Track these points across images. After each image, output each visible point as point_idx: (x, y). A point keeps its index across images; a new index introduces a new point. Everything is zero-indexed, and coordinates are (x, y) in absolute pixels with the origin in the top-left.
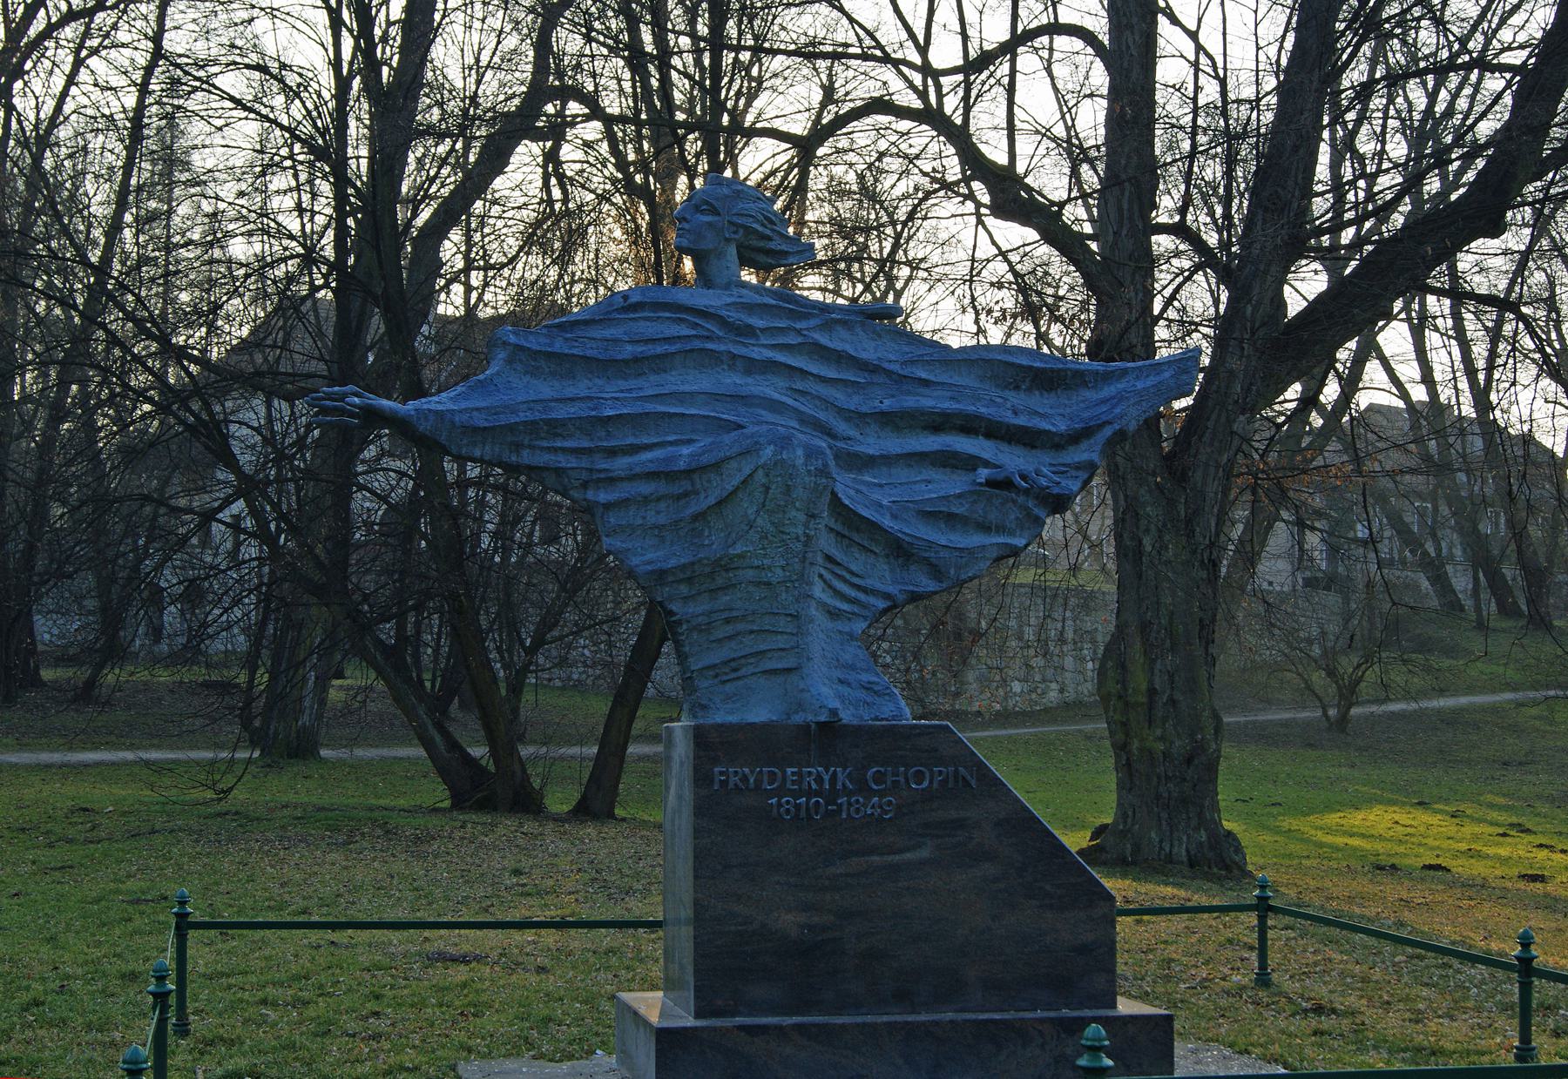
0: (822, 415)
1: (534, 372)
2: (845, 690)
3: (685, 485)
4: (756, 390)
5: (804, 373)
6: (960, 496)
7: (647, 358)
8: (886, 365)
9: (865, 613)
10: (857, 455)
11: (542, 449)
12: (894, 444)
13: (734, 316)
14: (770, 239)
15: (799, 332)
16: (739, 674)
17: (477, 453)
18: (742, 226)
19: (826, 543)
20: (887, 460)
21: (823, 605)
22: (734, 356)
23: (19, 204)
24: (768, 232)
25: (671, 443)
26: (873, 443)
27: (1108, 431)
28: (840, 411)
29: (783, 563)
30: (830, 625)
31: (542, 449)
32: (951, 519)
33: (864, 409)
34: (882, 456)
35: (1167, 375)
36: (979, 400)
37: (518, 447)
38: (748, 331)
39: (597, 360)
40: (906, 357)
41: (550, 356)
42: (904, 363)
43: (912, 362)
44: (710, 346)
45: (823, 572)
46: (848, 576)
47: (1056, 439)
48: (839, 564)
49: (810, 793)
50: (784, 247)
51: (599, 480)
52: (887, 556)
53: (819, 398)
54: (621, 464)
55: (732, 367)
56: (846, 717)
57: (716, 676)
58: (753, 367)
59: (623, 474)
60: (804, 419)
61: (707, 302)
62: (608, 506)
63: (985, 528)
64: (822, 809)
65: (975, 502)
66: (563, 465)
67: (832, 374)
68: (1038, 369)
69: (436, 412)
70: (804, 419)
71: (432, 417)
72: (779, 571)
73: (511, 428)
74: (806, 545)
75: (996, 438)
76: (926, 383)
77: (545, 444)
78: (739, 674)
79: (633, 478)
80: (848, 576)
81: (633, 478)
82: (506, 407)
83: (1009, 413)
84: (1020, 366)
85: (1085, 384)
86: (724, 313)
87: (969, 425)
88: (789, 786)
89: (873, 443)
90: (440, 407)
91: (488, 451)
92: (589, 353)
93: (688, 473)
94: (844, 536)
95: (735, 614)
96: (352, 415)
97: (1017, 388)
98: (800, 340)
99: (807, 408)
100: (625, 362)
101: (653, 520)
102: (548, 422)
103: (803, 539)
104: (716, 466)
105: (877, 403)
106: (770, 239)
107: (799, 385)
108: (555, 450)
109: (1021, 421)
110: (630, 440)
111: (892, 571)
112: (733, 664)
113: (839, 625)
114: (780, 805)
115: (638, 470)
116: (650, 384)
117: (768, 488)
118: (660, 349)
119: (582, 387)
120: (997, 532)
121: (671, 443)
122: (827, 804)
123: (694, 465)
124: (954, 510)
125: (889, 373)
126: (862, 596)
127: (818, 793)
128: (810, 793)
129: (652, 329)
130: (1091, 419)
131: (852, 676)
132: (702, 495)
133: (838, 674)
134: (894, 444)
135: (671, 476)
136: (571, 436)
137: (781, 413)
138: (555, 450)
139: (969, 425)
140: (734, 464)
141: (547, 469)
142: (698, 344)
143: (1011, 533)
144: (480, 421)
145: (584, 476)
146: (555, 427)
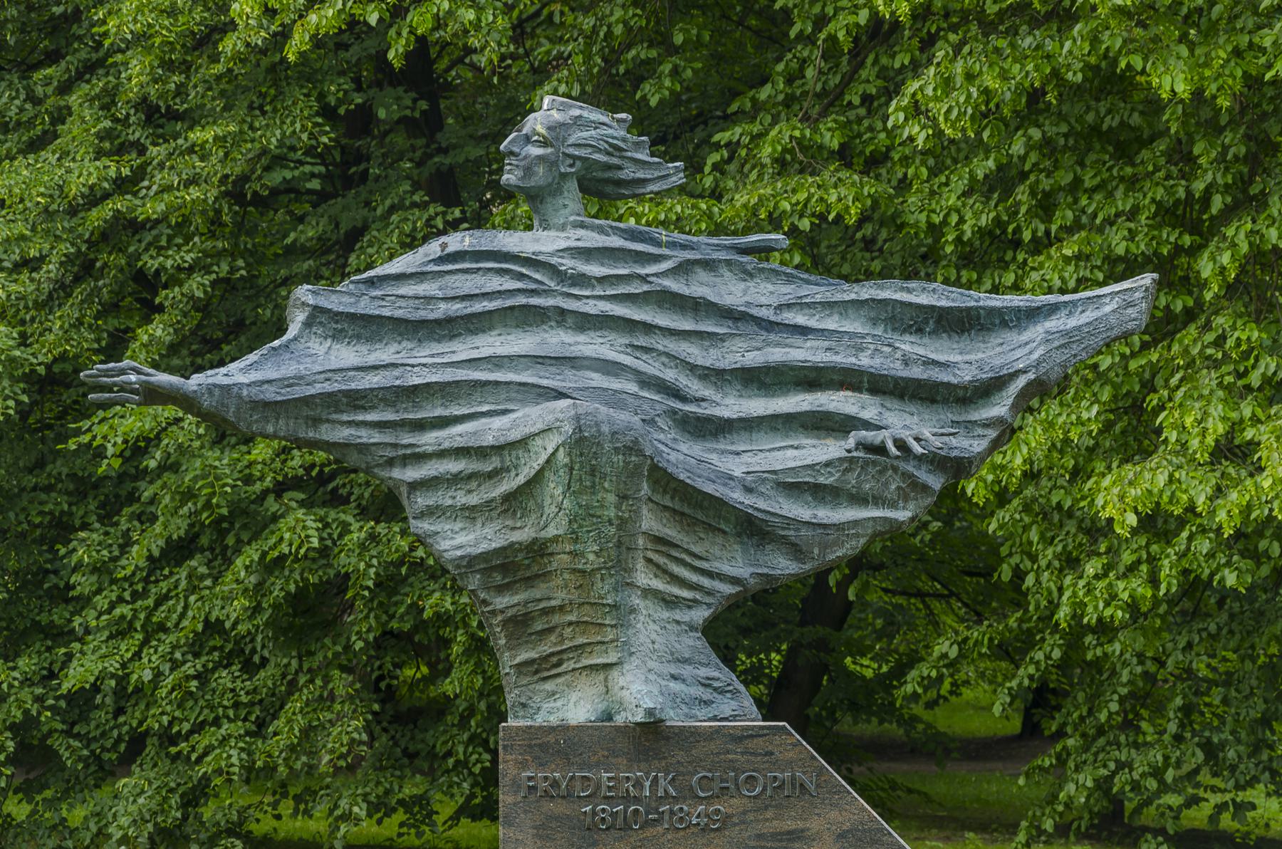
0: (670, 375)
1: (337, 336)
2: (675, 686)
3: (493, 463)
4: (589, 351)
5: (648, 328)
6: (828, 464)
7: (462, 317)
8: (754, 311)
9: (708, 600)
10: (709, 419)
11: (343, 423)
12: (758, 406)
13: (567, 264)
14: (620, 168)
15: (644, 279)
16: (559, 670)
17: (270, 429)
18: (579, 158)
19: (649, 521)
20: (750, 425)
21: (648, 593)
22: (562, 312)
23: (39, 714)
24: (615, 161)
25: (483, 414)
26: (733, 405)
27: (1021, 382)
28: (693, 368)
29: (596, 548)
30: (666, 614)
31: (343, 423)
32: (818, 492)
33: (721, 365)
34: (741, 420)
35: (1108, 309)
36: (862, 350)
37: (316, 422)
38: (581, 280)
39: (406, 321)
40: (783, 300)
41: (353, 317)
42: (780, 308)
43: (789, 306)
44: (535, 301)
45: (650, 555)
46: (688, 559)
47: (961, 393)
48: (677, 546)
49: (627, 799)
50: (640, 175)
51: (405, 457)
52: (739, 535)
53: (667, 355)
54: (429, 440)
55: (561, 324)
56: (675, 718)
57: (536, 672)
58: (586, 323)
59: (430, 449)
60: (647, 382)
61: (537, 248)
62: (414, 486)
63: (859, 499)
64: (641, 819)
65: (847, 470)
66: (364, 440)
67: (688, 325)
68: (940, 308)
69: (221, 387)
70: (647, 382)
71: (217, 392)
72: (591, 557)
73: (307, 401)
74: (619, 528)
75: (884, 393)
76: (803, 331)
77: (345, 417)
78: (559, 670)
79: (442, 454)
80: (688, 559)
81: (442, 454)
82: (301, 378)
83: (898, 365)
84: (919, 307)
85: (1005, 324)
86: (554, 260)
87: (849, 379)
88: (604, 791)
89: (733, 405)
90: (226, 381)
91: (283, 426)
92: (398, 313)
93: (498, 449)
94: (683, 514)
95: (553, 603)
96: (133, 392)
97: (920, 331)
98: (646, 288)
99: (651, 367)
100: (437, 322)
101: (464, 500)
102: (348, 394)
103: (616, 522)
104: (523, 443)
105: (738, 357)
106: (620, 168)
107: (642, 341)
108: (358, 424)
109: (917, 372)
110: (439, 412)
111: (745, 551)
112: (555, 659)
113: (678, 615)
114: (594, 813)
115: (446, 445)
116: (463, 349)
117: (572, 469)
118: (479, 307)
119: (385, 353)
120: (876, 504)
121: (483, 414)
122: (647, 813)
123: (502, 440)
124: (821, 480)
125: (758, 321)
126: (706, 582)
127: (637, 800)
128: (627, 799)
129: (468, 284)
130: (1001, 367)
131: (687, 671)
132: (513, 473)
133: (673, 669)
134: (758, 406)
135: (482, 452)
136: (373, 408)
137: (616, 375)
138: (358, 424)
139: (849, 379)
140: (539, 441)
141: (347, 445)
142: (521, 300)
143: (893, 505)
144: (270, 394)
145: (390, 453)
146: (357, 400)
